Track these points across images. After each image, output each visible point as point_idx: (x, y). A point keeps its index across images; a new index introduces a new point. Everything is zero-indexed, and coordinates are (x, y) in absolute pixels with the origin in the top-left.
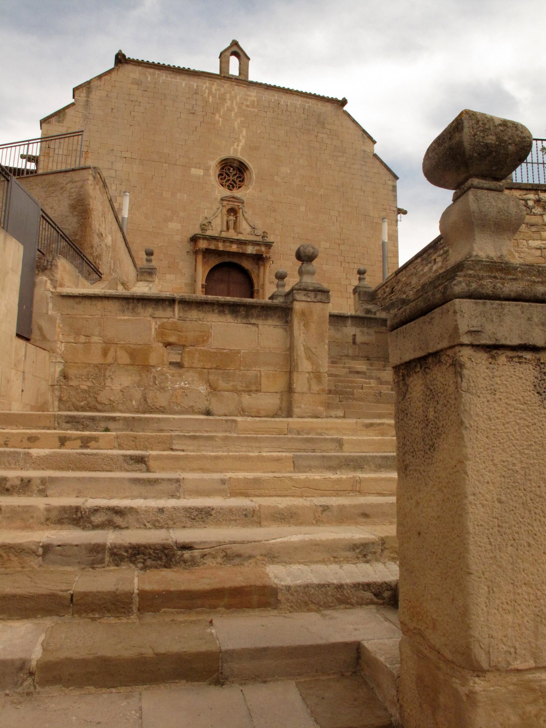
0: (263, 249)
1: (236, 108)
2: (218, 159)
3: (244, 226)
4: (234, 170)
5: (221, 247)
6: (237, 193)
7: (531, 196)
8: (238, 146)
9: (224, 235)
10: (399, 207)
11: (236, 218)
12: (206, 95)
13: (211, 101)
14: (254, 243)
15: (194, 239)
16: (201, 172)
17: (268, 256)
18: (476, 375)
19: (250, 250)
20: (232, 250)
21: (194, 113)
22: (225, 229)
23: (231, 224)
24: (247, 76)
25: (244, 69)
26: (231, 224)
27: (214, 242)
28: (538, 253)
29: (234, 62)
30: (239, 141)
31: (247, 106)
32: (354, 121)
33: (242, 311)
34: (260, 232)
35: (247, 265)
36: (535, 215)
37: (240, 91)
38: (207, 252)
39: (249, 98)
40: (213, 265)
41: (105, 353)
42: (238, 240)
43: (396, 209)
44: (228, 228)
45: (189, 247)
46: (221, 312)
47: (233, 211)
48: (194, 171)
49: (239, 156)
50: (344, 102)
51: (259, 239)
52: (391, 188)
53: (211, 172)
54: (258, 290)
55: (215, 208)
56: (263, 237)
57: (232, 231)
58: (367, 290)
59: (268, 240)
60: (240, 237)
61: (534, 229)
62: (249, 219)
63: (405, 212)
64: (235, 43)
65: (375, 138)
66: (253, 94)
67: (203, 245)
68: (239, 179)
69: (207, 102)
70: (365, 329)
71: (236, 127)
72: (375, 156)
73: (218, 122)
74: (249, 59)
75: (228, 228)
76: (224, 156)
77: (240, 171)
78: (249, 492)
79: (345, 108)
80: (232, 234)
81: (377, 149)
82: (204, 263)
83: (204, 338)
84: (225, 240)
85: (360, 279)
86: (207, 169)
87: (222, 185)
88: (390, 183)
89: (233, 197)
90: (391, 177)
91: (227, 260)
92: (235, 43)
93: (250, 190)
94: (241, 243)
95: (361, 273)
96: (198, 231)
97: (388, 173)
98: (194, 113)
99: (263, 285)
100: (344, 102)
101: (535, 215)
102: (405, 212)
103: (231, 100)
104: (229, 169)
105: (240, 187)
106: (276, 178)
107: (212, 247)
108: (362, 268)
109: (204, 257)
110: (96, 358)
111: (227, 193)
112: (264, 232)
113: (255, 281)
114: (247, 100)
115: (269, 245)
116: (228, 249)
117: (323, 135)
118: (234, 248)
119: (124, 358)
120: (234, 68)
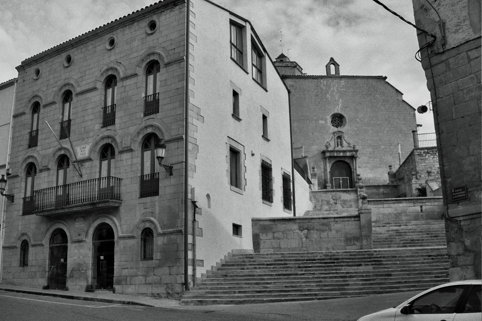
0: (354, 153)
1: (336, 90)
2: (331, 114)
3: (345, 143)
4: (338, 118)
5: (335, 154)
6: (339, 129)
7: (423, 151)
8: (338, 107)
9: (337, 149)
10: (417, 124)
11: (341, 140)
12: (322, 86)
13: (324, 88)
14: (350, 151)
15: (324, 152)
16: (324, 122)
17: (357, 156)
18: (36, 193)
19: (348, 154)
20: (340, 155)
21: (317, 96)
22: (336, 146)
23: (339, 143)
24: (339, 74)
25: (337, 70)
26: (339, 143)
27: (332, 153)
28: (424, 167)
29: (332, 67)
30: (338, 105)
31: (341, 88)
32: (391, 86)
33: (347, 192)
34: (352, 145)
35: (348, 161)
36: (423, 156)
37: (336, 81)
38: (330, 157)
39: (341, 84)
40: (333, 162)
41: (322, 202)
42: (343, 151)
43: (416, 125)
44: (338, 145)
45: (321, 156)
46: (343, 192)
47: (339, 137)
48: (321, 122)
49: (339, 112)
50: (386, 78)
51: (352, 149)
52: (413, 115)
53: (328, 121)
54: (354, 172)
55: (331, 137)
56: (354, 148)
57: (340, 146)
58: (392, 173)
59: (356, 149)
60: (344, 149)
61: (423, 160)
62: (347, 140)
63: (421, 126)
64: (332, 59)
65: (402, 93)
66: (343, 82)
67: (328, 154)
68: (341, 122)
69: (323, 89)
70: (387, 189)
71: (337, 99)
72: (403, 101)
73: (329, 97)
74: (339, 66)
75: (338, 145)
76: (333, 113)
77: (341, 118)
78: (273, 223)
79: (387, 80)
80: (339, 148)
81: (404, 98)
82: (329, 162)
83: (340, 197)
84: (337, 151)
85: (390, 169)
86: (326, 120)
87: (333, 126)
88: (412, 113)
89: (339, 131)
90: (412, 110)
91: (339, 159)
92: (332, 59)
93: (346, 127)
94: (344, 152)
95: (390, 166)
96: (325, 149)
97: (411, 108)
98: (317, 96)
99: (356, 169)
100: (386, 78)
101: (423, 156)
102: (421, 126)
103: (333, 87)
104: (336, 118)
105: (341, 126)
106: (357, 119)
107: (332, 155)
108: (390, 165)
109: (329, 160)
110: (320, 203)
111: (336, 129)
112: (354, 146)
113: (352, 167)
114: (340, 85)
115: (357, 151)
116: (339, 155)
117: (377, 96)
118: (341, 154)
119: (326, 203)
120: (333, 72)
